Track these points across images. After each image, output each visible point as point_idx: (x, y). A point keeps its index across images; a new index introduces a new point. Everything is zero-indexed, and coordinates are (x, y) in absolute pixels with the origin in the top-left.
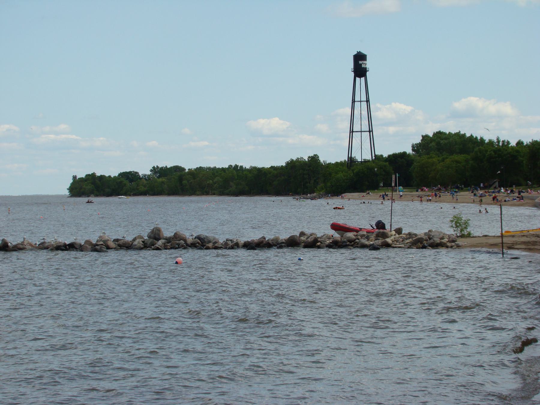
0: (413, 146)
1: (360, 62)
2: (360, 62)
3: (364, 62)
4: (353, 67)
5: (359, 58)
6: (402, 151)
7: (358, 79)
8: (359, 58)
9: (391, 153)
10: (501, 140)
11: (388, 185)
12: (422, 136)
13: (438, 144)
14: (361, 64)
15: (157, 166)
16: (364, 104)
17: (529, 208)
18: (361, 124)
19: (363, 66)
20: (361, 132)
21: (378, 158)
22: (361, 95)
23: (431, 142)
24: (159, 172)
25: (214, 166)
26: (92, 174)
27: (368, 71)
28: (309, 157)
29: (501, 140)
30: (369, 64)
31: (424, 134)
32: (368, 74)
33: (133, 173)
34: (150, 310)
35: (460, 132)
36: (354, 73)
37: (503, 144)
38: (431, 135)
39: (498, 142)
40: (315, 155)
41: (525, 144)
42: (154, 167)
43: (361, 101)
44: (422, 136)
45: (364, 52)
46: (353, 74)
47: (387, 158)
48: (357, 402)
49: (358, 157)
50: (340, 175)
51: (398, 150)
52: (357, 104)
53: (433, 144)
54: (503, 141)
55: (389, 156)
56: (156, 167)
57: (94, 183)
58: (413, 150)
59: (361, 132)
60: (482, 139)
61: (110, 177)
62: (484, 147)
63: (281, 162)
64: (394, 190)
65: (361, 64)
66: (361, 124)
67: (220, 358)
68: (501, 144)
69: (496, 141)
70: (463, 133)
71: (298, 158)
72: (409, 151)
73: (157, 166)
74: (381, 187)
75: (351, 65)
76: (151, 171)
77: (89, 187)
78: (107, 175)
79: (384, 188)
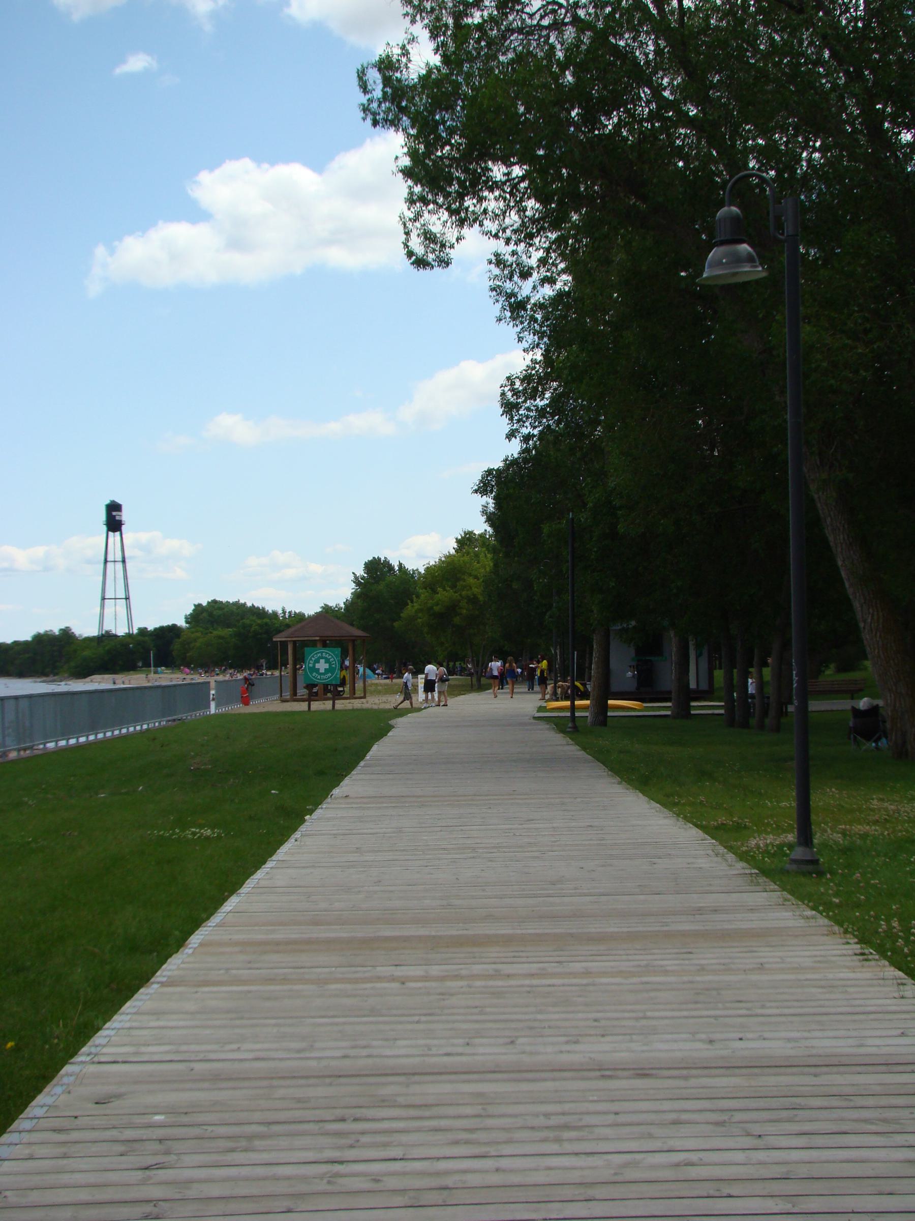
0: (186, 618)
1: (114, 513)
3: (119, 513)
5: (113, 508)
6: (170, 623)
7: (111, 534)
8: (113, 508)
9: (157, 626)
10: (287, 611)
11: (147, 665)
12: (195, 605)
13: (211, 615)
14: (115, 516)
16: (120, 566)
18: (115, 589)
19: (117, 518)
21: (143, 631)
23: (202, 613)
24: (43, 642)
28: (61, 630)
29: (287, 611)
30: (125, 516)
31: (196, 603)
32: (123, 527)
33: (778, 883)
35: (239, 601)
37: (290, 616)
38: (205, 604)
39: (284, 612)
40: (67, 627)
41: (307, 616)
44: (195, 605)
46: (105, 528)
47: (152, 632)
48: (358, 1141)
50: (87, 653)
51: (166, 622)
52: (110, 566)
53: (205, 614)
54: (290, 612)
55: (156, 629)
58: (187, 622)
60: (263, 609)
61: (227, 602)
63: (26, 635)
64: (578, 695)
66: (115, 589)
67: (53, 1099)
68: (287, 616)
69: (280, 611)
70: (243, 602)
71: (47, 631)
72: (181, 623)
74: (139, 667)
79: (144, 668)
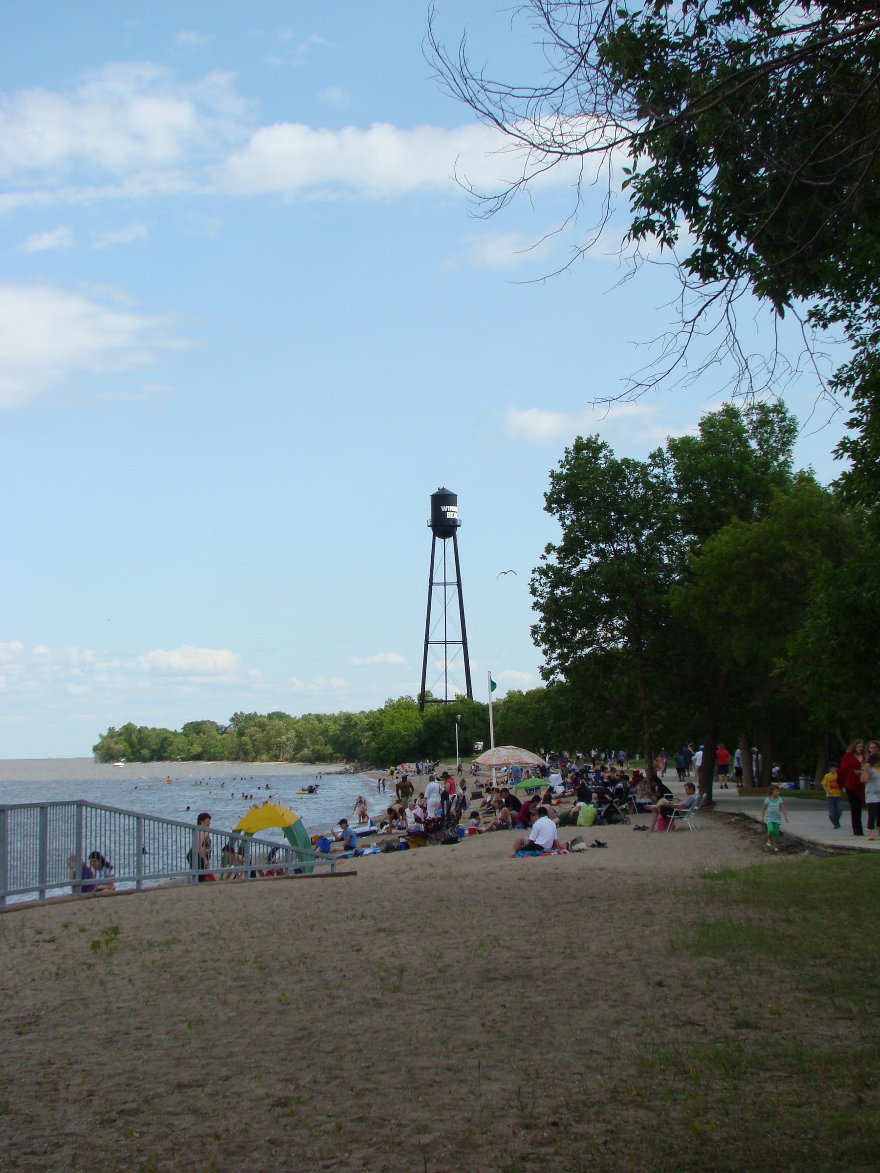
1: (444, 508)
2: (444, 508)
4: (430, 518)
5: (442, 499)
14: (445, 513)
15: (241, 713)
17: (728, 798)
19: (449, 515)
20: (446, 643)
22: (445, 572)
25: (331, 713)
26: (128, 725)
27: (459, 526)
32: (459, 531)
34: (475, 1062)
36: (433, 530)
42: (236, 714)
43: (445, 584)
45: (451, 489)
46: (430, 532)
49: (437, 691)
52: (437, 590)
56: (239, 713)
57: (129, 741)
59: (446, 643)
62: (780, 668)
65: (445, 513)
73: (241, 713)
75: (427, 514)
76: (232, 720)
77: (122, 747)
78: (150, 727)
